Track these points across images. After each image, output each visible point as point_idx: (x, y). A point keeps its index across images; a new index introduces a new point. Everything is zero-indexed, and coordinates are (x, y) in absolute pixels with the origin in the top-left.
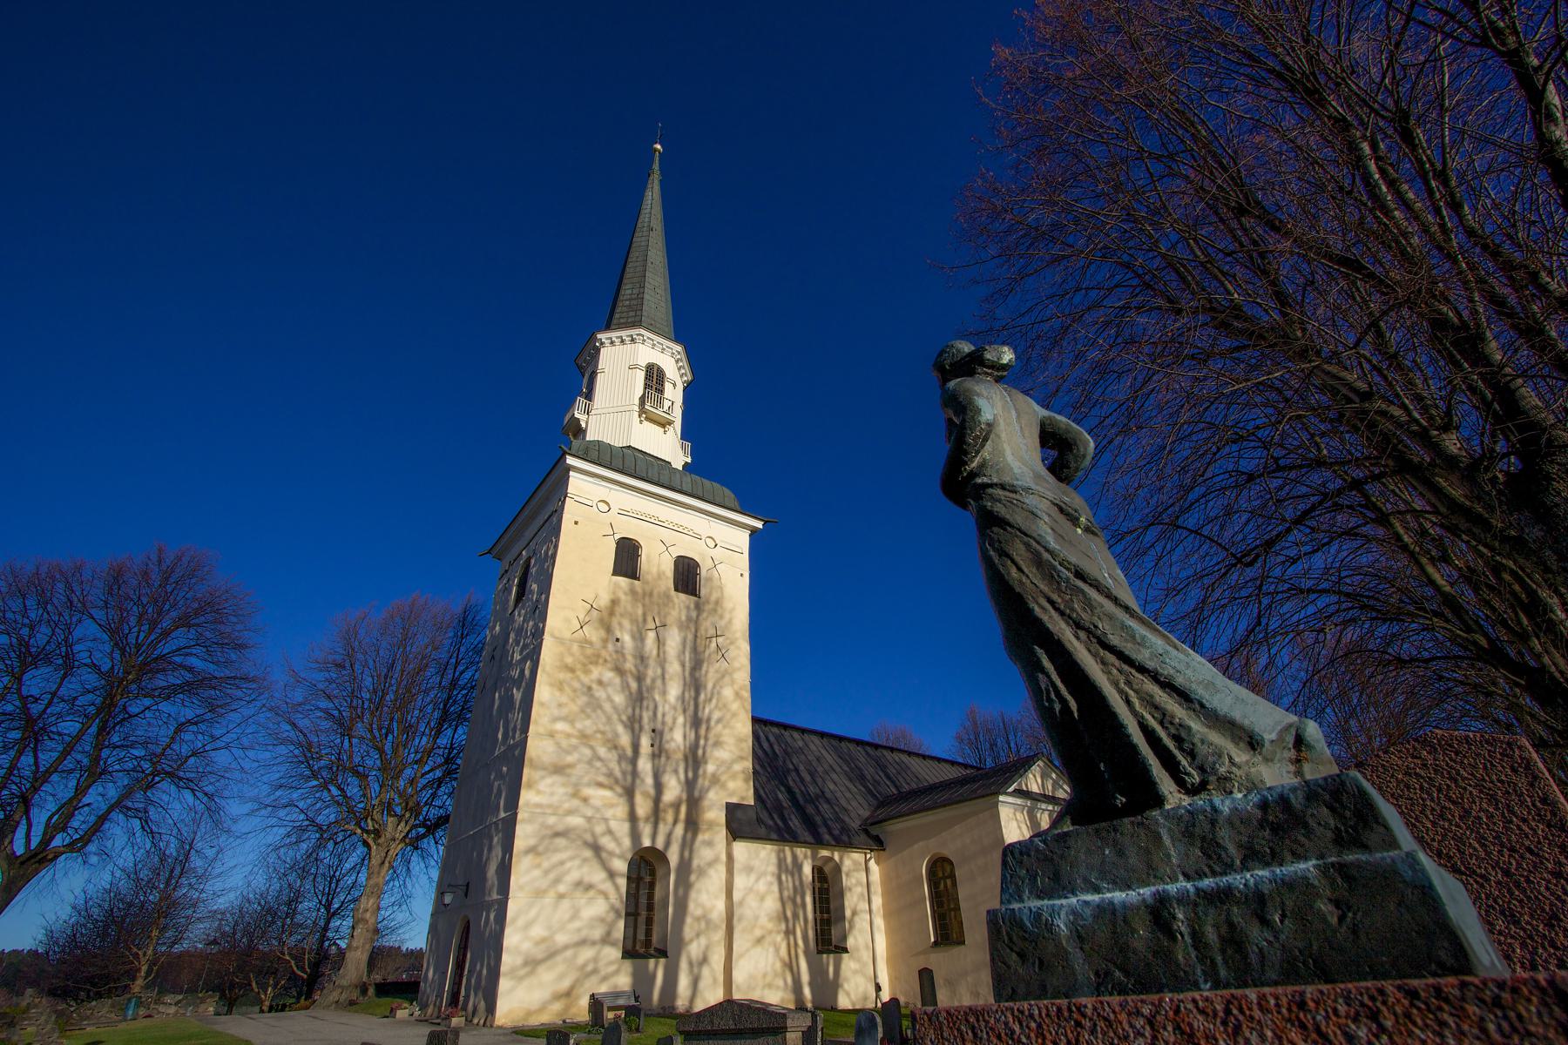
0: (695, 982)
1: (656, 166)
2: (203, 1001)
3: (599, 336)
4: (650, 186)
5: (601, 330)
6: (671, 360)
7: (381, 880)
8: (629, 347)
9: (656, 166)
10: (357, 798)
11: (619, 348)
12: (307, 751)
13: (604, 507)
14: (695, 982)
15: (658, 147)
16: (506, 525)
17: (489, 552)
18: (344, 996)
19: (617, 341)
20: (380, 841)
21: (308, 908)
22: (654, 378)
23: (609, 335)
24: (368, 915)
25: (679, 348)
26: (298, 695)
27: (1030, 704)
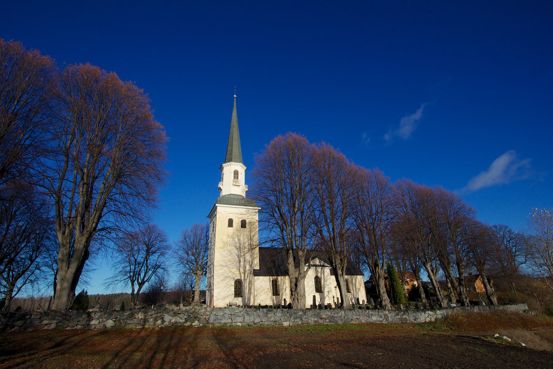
0: (254, 300)
1: (235, 100)
2: (172, 305)
3: (223, 165)
4: (233, 111)
5: (223, 163)
6: (241, 168)
7: (198, 283)
8: (230, 166)
9: (235, 100)
10: (89, 153)
11: (228, 167)
12: (181, 258)
13: (225, 213)
14: (254, 300)
15: (235, 96)
16: (210, 211)
17: (208, 217)
18: (195, 304)
19: (229, 165)
20: (197, 275)
21: (188, 286)
22: (236, 173)
23: (225, 164)
24: (197, 289)
25: (241, 164)
26: (177, 248)
27: (48, 306)
